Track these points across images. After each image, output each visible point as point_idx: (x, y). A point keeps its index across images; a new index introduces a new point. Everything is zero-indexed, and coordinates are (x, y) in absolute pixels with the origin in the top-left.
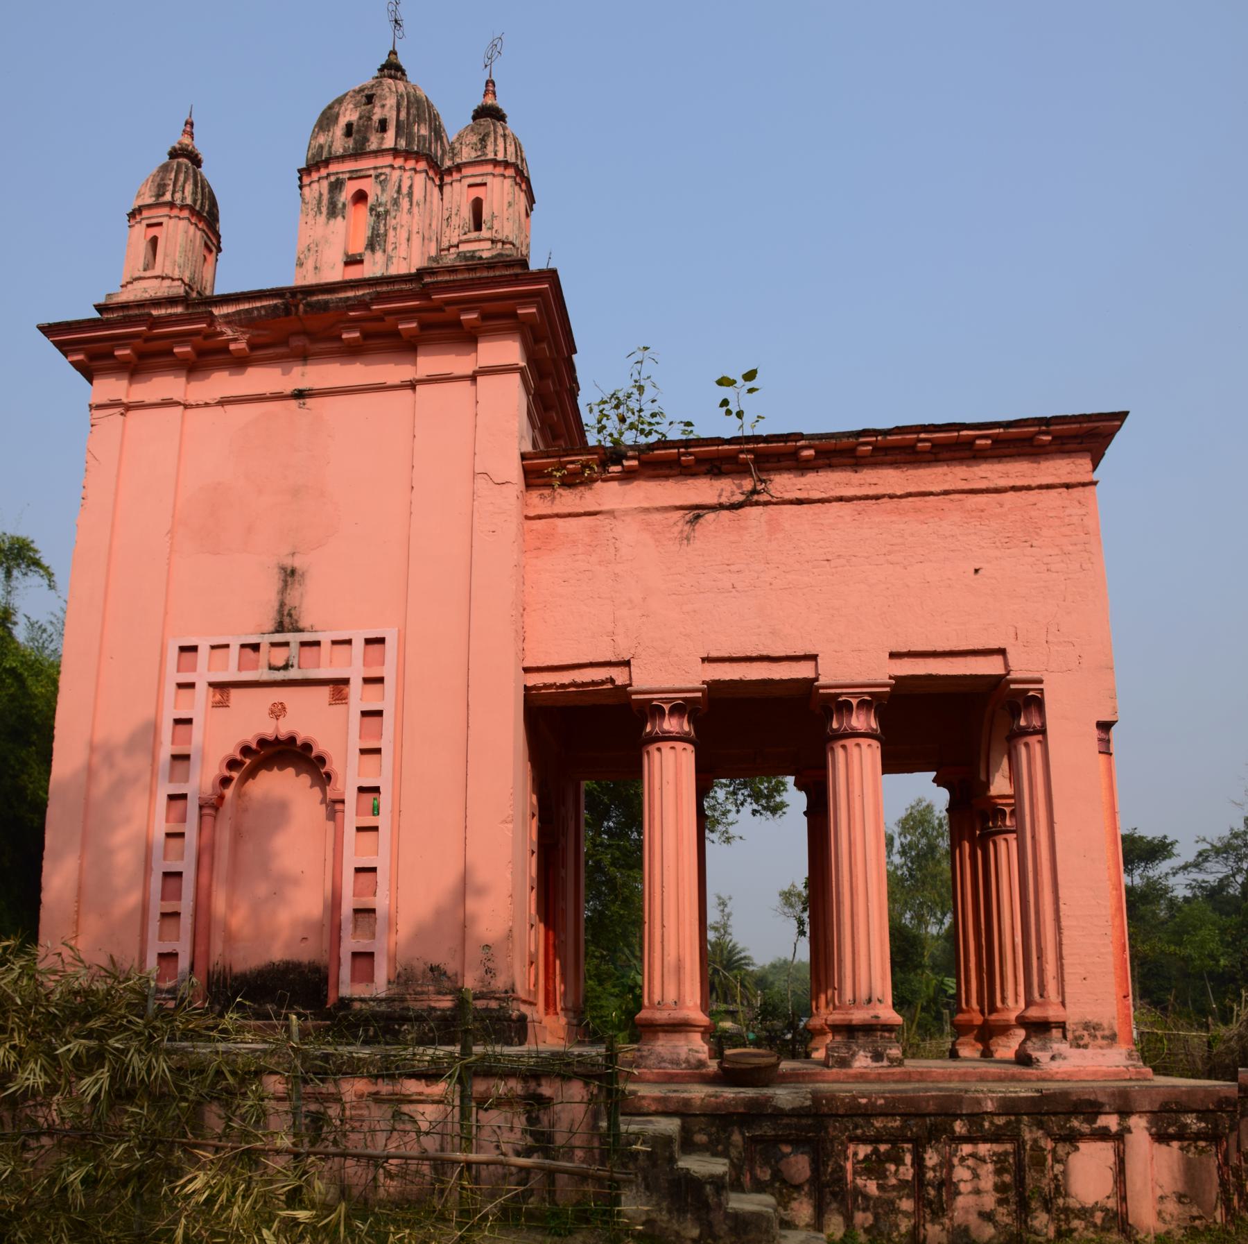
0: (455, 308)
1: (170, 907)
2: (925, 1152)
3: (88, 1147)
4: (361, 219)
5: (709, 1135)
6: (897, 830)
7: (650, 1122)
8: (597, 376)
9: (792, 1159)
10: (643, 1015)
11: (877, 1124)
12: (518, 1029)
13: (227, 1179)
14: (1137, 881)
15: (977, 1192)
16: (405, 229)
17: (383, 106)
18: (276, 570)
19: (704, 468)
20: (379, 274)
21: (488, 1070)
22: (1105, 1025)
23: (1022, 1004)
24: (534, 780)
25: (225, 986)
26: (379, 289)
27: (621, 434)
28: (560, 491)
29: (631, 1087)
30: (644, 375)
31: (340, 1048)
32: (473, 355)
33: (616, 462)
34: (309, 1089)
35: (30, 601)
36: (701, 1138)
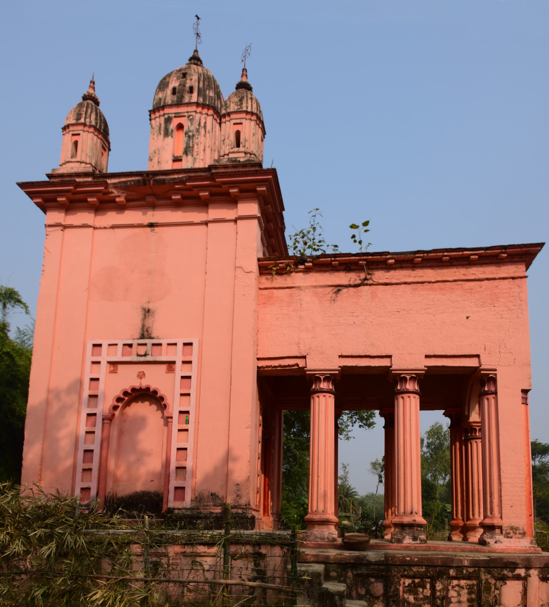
0: (227, 186)
1: (87, 466)
2: (436, 583)
3: (45, 579)
4: (180, 139)
5: (337, 573)
6: (426, 436)
7: (311, 566)
8: (294, 222)
9: (375, 584)
10: (308, 516)
11: (414, 570)
12: (251, 522)
13: (112, 593)
14: (537, 463)
15: (459, 602)
16: (203, 144)
17: (191, 79)
18: (141, 310)
19: (342, 267)
20: (189, 167)
21: (237, 541)
22: (521, 528)
23: (482, 517)
24: (261, 409)
25: (113, 503)
26: (190, 175)
27: (305, 250)
28: (275, 276)
29: (302, 550)
30: (316, 222)
31: (168, 531)
32: (236, 210)
33: (300, 263)
34: (153, 550)
35: (16, 321)
36: (333, 574)
